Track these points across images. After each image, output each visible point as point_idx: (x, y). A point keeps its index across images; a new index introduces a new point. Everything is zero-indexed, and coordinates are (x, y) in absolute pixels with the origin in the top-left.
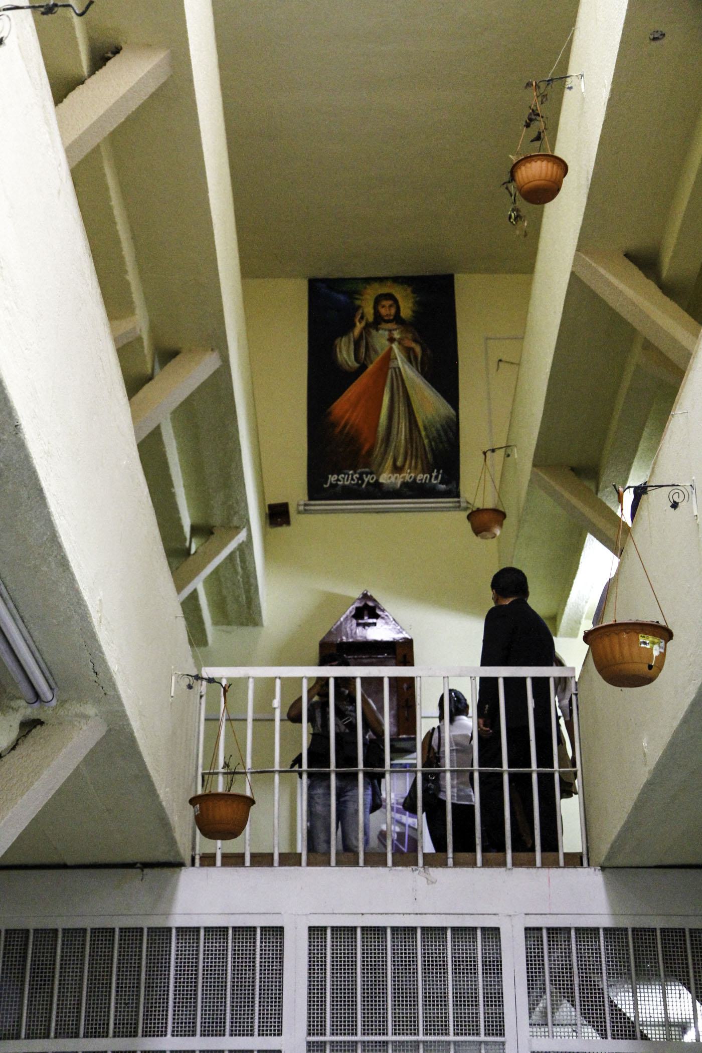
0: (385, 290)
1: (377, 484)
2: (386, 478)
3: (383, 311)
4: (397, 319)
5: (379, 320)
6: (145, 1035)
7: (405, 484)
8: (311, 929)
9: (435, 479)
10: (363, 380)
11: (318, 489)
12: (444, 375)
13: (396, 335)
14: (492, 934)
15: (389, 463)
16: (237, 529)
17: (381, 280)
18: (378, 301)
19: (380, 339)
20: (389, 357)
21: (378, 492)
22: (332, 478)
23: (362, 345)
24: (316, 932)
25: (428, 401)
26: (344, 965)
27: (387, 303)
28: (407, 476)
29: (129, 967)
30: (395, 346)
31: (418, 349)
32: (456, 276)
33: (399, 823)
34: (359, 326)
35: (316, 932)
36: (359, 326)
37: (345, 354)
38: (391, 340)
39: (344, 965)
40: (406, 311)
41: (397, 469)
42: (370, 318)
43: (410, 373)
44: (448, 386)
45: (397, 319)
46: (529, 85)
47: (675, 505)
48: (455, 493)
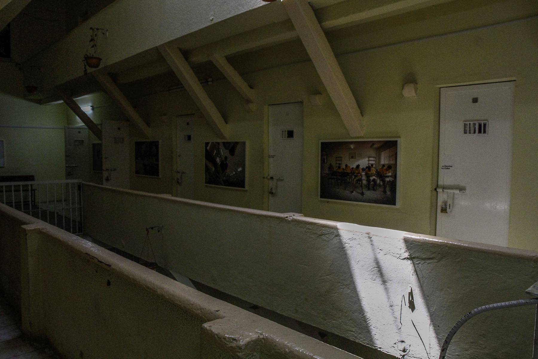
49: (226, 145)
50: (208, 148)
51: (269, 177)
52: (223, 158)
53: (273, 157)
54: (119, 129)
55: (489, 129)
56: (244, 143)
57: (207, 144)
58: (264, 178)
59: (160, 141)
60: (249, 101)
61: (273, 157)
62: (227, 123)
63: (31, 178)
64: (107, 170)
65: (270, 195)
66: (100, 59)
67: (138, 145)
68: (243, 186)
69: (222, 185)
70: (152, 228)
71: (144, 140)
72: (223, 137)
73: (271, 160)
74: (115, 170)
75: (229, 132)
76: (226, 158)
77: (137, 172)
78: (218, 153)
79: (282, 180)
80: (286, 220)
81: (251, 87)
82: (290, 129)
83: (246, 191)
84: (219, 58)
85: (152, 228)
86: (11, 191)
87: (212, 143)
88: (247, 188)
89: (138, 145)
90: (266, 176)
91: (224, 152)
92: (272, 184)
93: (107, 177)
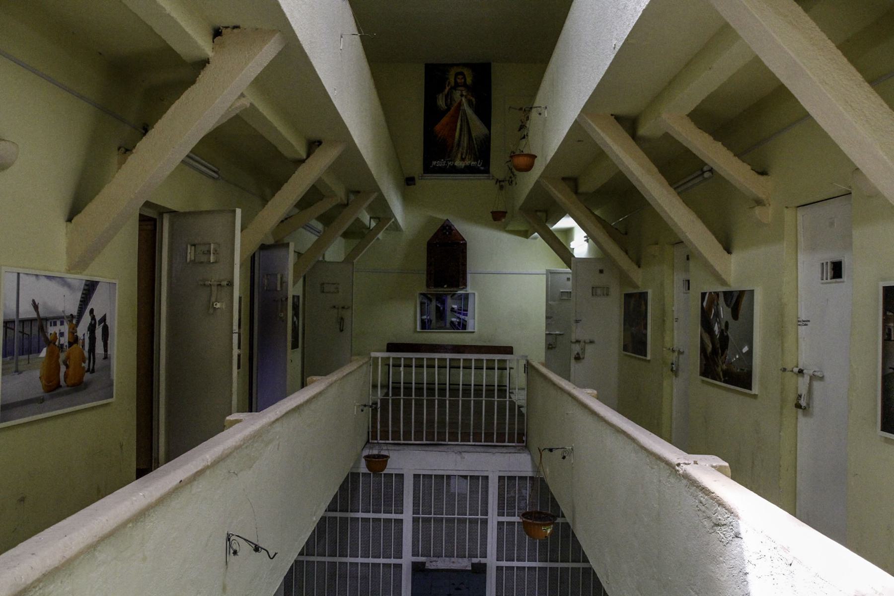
0: (459, 70)
1: (454, 166)
2: (458, 163)
3: (459, 81)
4: (465, 85)
5: (456, 86)
6: (351, 511)
7: (466, 166)
8: (415, 475)
9: (479, 164)
10: (448, 115)
11: (428, 169)
12: (484, 112)
13: (464, 93)
14: (486, 478)
15: (459, 155)
16: (390, 219)
17: (458, 65)
18: (457, 74)
19: (457, 95)
20: (460, 104)
21: (454, 170)
22: (434, 163)
23: (449, 97)
24: (416, 476)
25: (477, 127)
26: (426, 530)
27: (460, 77)
28: (467, 163)
29: (344, 532)
30: (464, 100)
31: (474, 100)
32: (493, 64)
33: (459, 318)
34: (447, 88)
35: (416, 476)
36: (447, 88)
37: (441, 102)
38: (462, 95)
39: (426, 530)
40: (469, 80)
41: (463, 159)
42: (453, 83)
43: (469, 112)
44: (486, 120)
45: (465, 85)
46: (521, 109)
47: (564, 458)
48: (487, 171)
49: (728, 295)
50: (705, 304)
51: (796, 370)
52: (723, 324)
53: (805, 323)
54: (601, 271)
55: (602, 275)
56: (752, 292)
57: (703, 295)
58: (784, 370)
59: (650, 292)
60: (759, 202)
61: (805, 323)
62: (729, 252)
63: (509, 350)
64: (578, 341)
65: (800, 411)
66: (534, 157)
67: (628, 296)
68: (749, 386)
69: (720, 381)
70: (551, 450)
71: (635, 291)
72: (724, 283)
73: (802, 329)
74: (591, 342)
75: (734, 270)
76: (727, 324)
77: (625, 348)
78: (717, 314)
79: (822, 378)
80: (674, 468)
81: (763, 173)
82: (836, 258)
83: (755, 396)
84: (673, 121)
85: (551, 450)
86: (494, 369)
87: (710, 293)
88: (755, 390)
89: (628, 296)
90: (789, 367)
91: (724, 312)
92: (802, 384)
93: (578, 354)
